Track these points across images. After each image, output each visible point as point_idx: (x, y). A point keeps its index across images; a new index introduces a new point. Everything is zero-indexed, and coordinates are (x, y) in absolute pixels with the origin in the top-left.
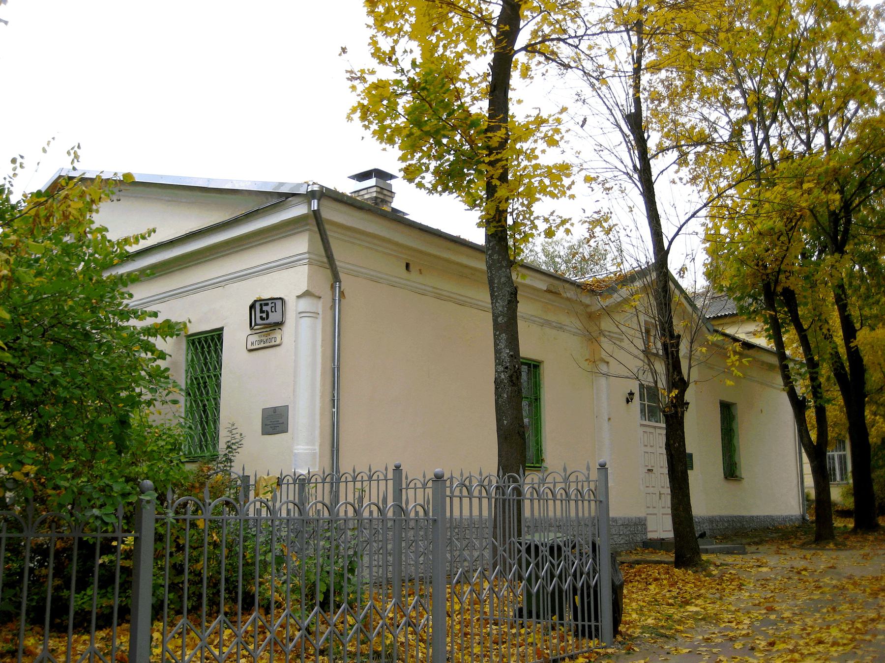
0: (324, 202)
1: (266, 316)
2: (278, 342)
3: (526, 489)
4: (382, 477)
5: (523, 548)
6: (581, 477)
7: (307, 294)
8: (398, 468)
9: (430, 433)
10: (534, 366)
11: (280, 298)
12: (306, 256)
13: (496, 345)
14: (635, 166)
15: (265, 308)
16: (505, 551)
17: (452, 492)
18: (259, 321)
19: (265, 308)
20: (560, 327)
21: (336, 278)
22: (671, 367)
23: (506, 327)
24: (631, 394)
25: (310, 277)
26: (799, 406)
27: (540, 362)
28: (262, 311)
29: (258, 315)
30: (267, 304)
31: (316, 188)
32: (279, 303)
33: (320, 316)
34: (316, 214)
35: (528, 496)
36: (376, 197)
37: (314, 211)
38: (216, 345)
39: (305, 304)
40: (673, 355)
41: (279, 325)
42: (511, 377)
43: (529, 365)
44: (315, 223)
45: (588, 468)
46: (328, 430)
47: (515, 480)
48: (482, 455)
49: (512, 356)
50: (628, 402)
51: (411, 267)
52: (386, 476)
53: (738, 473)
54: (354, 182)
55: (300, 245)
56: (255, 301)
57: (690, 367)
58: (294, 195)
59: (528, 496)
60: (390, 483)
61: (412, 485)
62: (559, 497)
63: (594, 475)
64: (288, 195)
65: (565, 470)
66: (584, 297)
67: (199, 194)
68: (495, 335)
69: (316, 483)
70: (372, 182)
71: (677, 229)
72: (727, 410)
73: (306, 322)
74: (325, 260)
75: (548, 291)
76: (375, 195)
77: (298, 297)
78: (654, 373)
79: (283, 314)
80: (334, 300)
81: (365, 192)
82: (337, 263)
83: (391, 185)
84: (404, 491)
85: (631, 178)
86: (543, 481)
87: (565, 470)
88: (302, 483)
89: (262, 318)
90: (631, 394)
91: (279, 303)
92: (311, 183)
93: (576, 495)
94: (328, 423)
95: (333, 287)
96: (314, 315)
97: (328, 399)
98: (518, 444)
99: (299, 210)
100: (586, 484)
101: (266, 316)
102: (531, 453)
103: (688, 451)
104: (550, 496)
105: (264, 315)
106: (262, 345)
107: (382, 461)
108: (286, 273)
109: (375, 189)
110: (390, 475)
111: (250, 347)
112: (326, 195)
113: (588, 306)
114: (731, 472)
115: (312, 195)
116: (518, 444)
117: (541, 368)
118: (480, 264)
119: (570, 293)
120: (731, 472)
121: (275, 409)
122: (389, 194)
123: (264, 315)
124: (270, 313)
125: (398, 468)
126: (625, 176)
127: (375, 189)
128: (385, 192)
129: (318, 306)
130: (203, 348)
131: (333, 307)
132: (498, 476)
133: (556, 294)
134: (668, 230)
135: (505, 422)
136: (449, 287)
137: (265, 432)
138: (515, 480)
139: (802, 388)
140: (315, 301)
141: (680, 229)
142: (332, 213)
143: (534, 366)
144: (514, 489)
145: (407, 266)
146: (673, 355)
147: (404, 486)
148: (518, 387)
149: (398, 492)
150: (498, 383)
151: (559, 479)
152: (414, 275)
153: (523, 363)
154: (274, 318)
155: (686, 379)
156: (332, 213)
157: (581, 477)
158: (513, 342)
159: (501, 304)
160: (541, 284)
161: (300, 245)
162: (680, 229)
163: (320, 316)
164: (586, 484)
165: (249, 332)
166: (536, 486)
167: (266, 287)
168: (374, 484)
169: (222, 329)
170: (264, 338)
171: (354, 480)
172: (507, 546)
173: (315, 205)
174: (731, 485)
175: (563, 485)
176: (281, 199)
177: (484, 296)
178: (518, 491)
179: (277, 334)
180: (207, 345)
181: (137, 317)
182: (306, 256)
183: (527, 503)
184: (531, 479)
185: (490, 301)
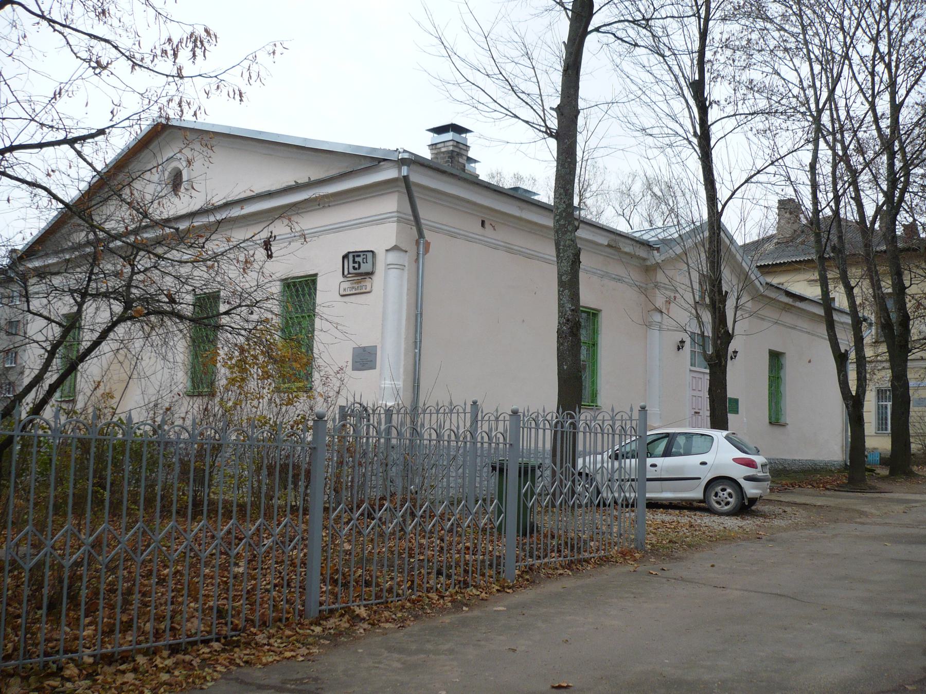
0: (413, 167)
1: (358, 267)
2: (368, 290)
3: (581, 425)
4: (461, 410)
5: (576, 473)
6: (625, 417)
7: (395, 248)
8: (475, 403)
9: (503, 376)
10: (593, 314)
11: (372, 252)
12: (395, 214)
13: (560, 300)
14: (695, 132)
15: (357, 259)
16: (562, 473)
17: (524, 424)
18: (352, 271)
19: (357, 259)
20: (619, 280)
21: (421, 234)
22: (717, 321)
23: (569, 284)
24: (682, 342)
25: (398, 233)
26: (841, 359)
27: (599, 311)
28: (354, 262)
29: (351, 265)
30: (359, 256)
31: (406, 156)
32: (370, 255)
33: (406, 268)
34: (406, 178)
35: (582, 429)
36: (452, 151)
37: (404, 177)
38: (310, 289)
39: (393, 257)
40: (720, 310)
41: (370, 274)
42: (571, 328)
43: (588, 313)
44: (404, 185)
45: (631, 410)
46: (410, 368)
47: (572, 417)
48: (542, 394)
49: (573, 310)
50: (679, 349)
51: (487, 225)
52: (464, 410)
53: (782, 421)
54: (431, 134)
55: (390, 204)
56: (349, 253)
57: (735, 322)
58: (385, 160)
59: (582, 429)
60: (468, 415)
61: (486, 418)
62: (606, 431)
63: (636, 415)
64: (380, 160)
65: (613, 410)
66: (638, 256)
67: (295, 150)
68: (559, 291)
69: (431, 414)
70: (449, 136)
71: (730, 193)
72: (776, 358)
73: (394, 273)
74: (412, 218)
75: (609, 246)
76: (451, 148)
77: (387, 250)
78: (701, 323)
79: (374, 264)
80: (418, 254)
81: (442, 145)
82: (422, 221)
83: (466, 139)
84: (479, 423)
85: (690, 142)
86: (595, 418)
87: (613, 410)
88: (389, 412)
89: (354, 268)
90: (682, 342)
91: (370, 255)
92: (401, 150)
93: (620, 431)
94: (411, 361)
95: (418, 243)
96: (401, 267)
97: (412, 340)
98: (574, 386)
99: (390, 173)
100: (628, 422)
101: (358, 267)
102: (586, 393)
103: (730, 395)
104: (599, 430)
105: (356, 266)
106: (354, 292)
107: (462, 398)
108: (376, 227)
109: (451, 143)
110: (468, 409)
111: (342, 293)
112: (414, 161)
113: (645, 260)
114: (776, 421)
115: (403, 162)
116: (574, 386)
117: (600, 316)
118: (549, 222)
119: (627, 248)
120: (776, 421)
121: (364, 349)
122: (465, 148)
123: (356, 266)
124: (362, 264)
125: (475, 403)
126: (686, 142)
127: (451, 143)
128: (461, 146)
129: (405, 259)
130: (297, 291)
131: (417, 260)
132: (558, 412)
133: (617, 249)
134: (722, 194)
135: (565, 367)
136: (519, 240)
137: (355, 368)
138: (572, 417)
139: (846, 341)
140: (402, 254)
141: (733, 194)
142: (418, 178)
143: (593, 314)
144: (571, 423)
145: (483, 223)
146: (720, 310)
147: (479, 418)
148: (576, 333)
149: (475, 421)
150: (559, 332)
151: (607, 417)
152: (489, 230)
153: (583, 311)
154: (365, 268)
155: (731, 332)
156: (418, 178)
157: (625, 417)
158: (575, 296)
159: (566, 266)
160: (603, 240)
161: (390, 204)
162: (733, 194)
163: (406, 268)
164: (628, 422)
165: (342, 279)
166: (588, 422)
167: (356, 242)
168: (454, 416)
169: (316, 275)
170: (356, 286)
171: (438, 412)
172: (564, 469)
173: (405, 171)
174: (777, 430)
175: (611, 422)
176: (372, 161)
177: (550, 251)
178: (574, 425)
179: (367, 283)
180: (301, 289)
181: (867, 516)
182: (395, 214)
183: (580, 436)
184: (585, 416)
185: (554, 254)
